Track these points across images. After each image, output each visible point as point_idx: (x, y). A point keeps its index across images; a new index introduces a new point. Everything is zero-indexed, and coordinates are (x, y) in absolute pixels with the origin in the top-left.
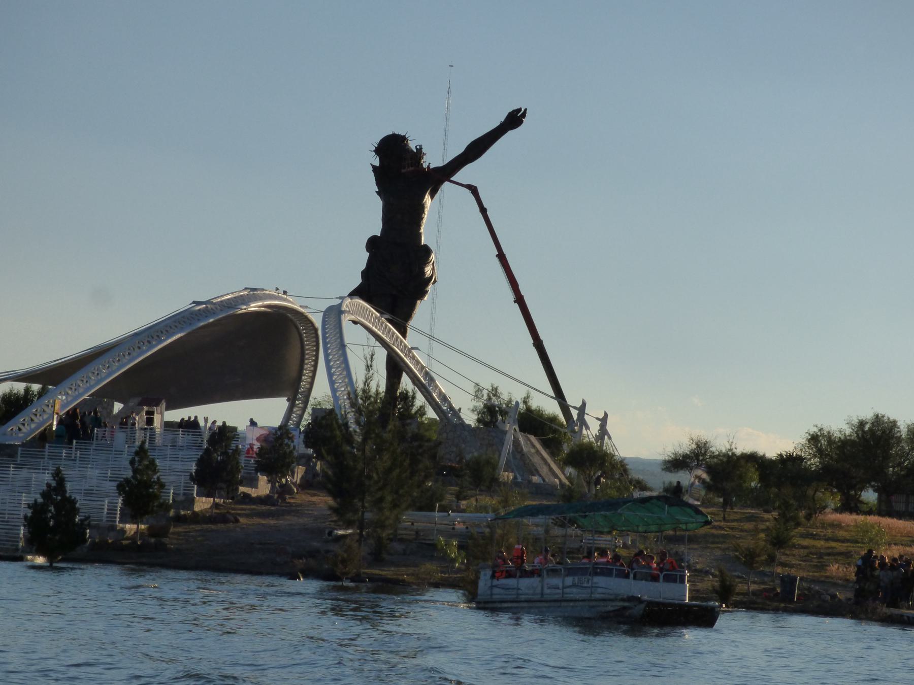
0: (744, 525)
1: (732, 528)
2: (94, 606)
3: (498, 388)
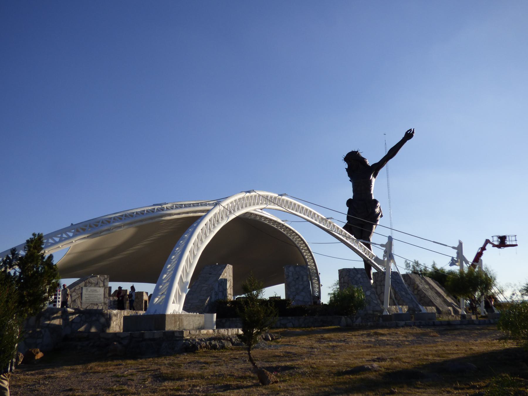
0: (200, 328)
1: (349, 335)
3: (419, 261)
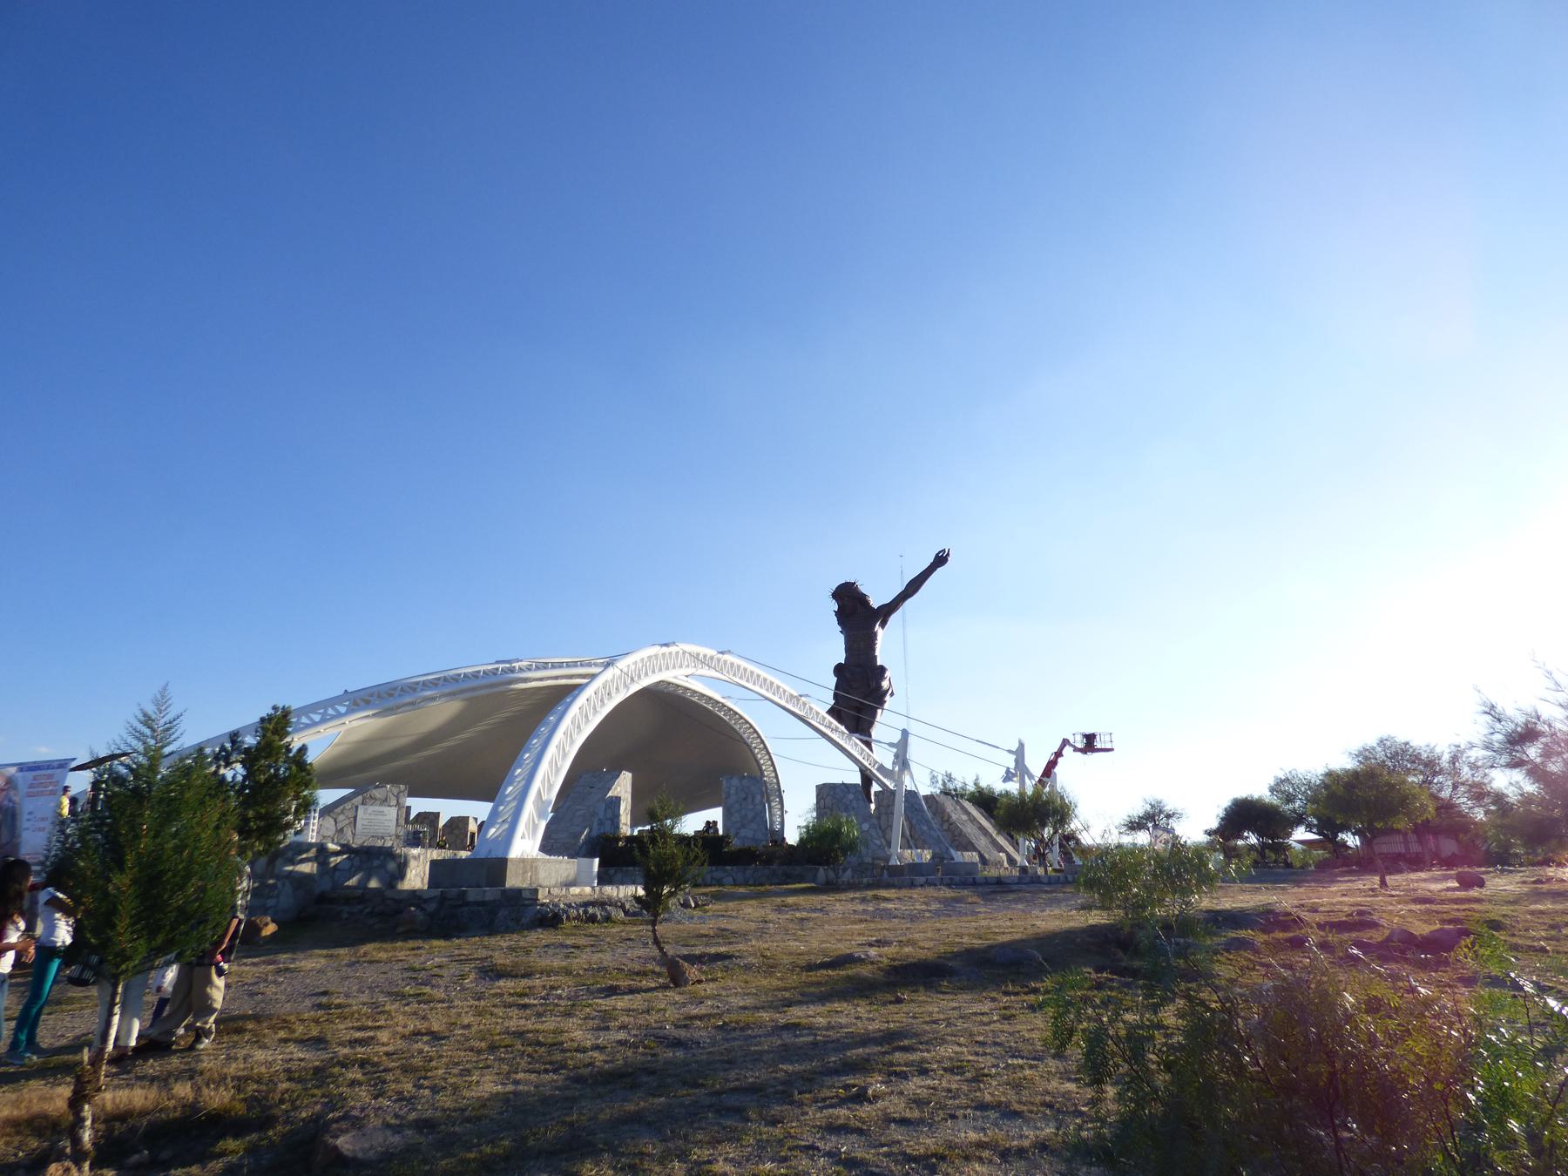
0: (569, 884)
2: (859, 944)
